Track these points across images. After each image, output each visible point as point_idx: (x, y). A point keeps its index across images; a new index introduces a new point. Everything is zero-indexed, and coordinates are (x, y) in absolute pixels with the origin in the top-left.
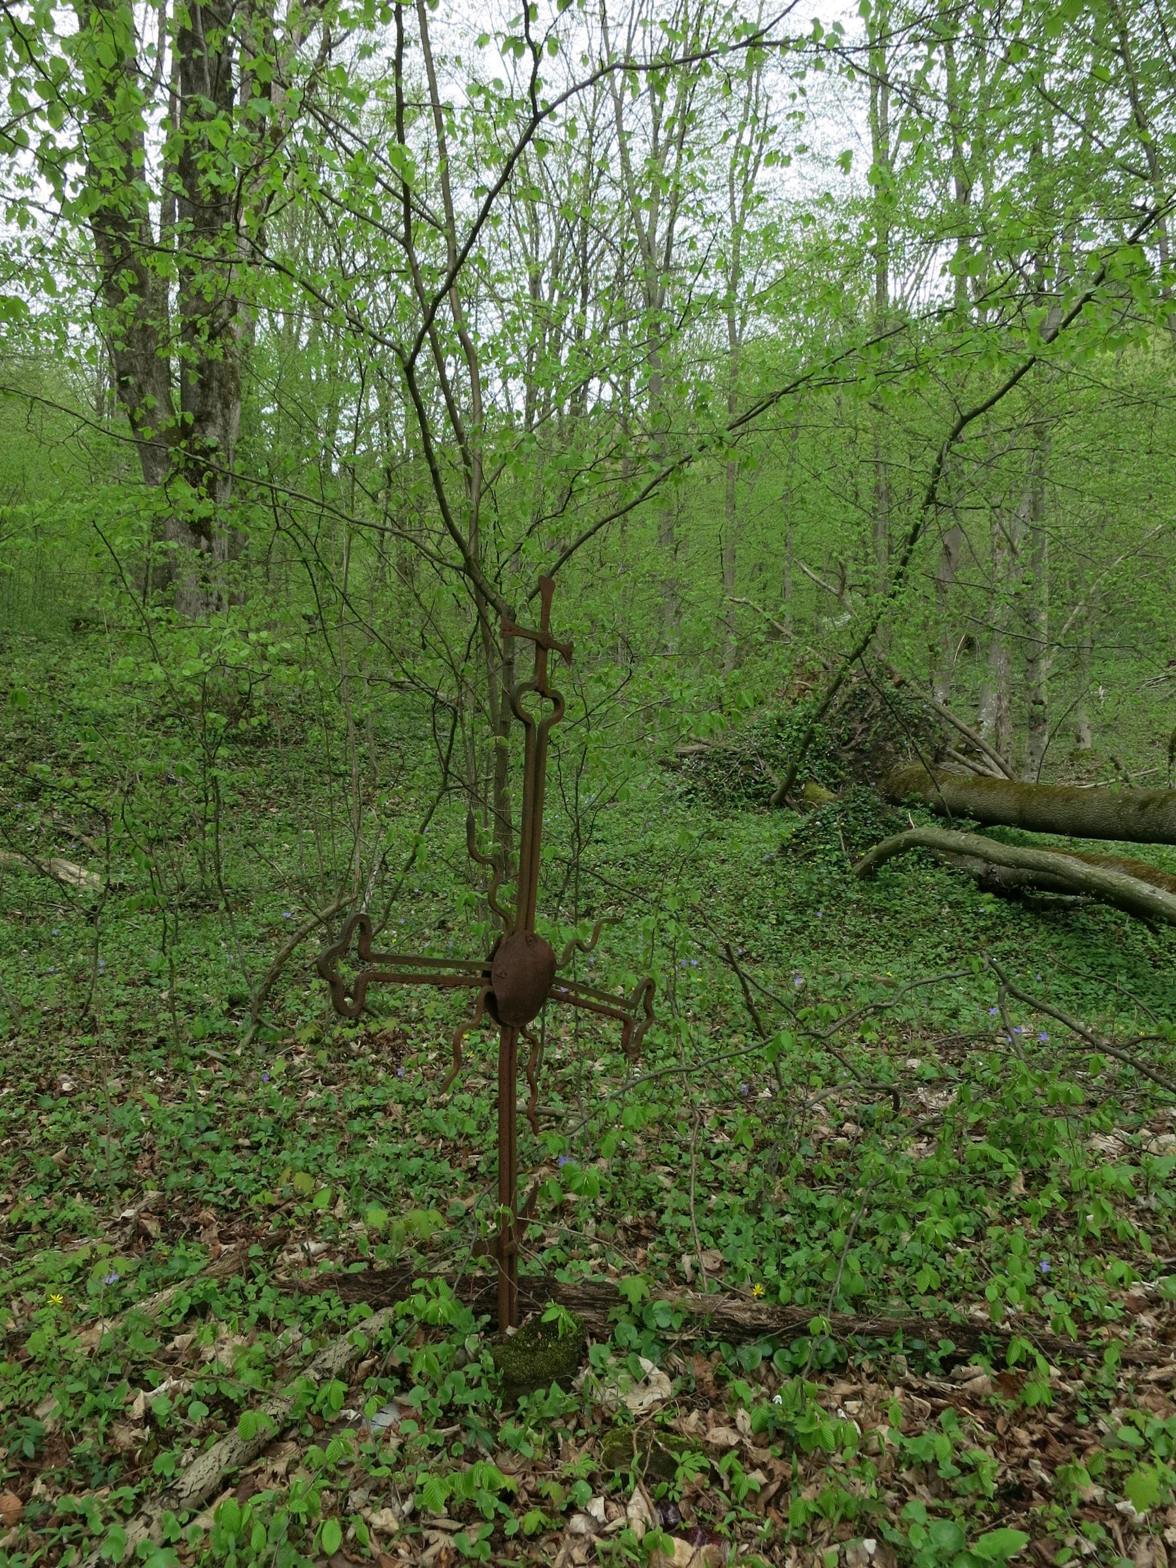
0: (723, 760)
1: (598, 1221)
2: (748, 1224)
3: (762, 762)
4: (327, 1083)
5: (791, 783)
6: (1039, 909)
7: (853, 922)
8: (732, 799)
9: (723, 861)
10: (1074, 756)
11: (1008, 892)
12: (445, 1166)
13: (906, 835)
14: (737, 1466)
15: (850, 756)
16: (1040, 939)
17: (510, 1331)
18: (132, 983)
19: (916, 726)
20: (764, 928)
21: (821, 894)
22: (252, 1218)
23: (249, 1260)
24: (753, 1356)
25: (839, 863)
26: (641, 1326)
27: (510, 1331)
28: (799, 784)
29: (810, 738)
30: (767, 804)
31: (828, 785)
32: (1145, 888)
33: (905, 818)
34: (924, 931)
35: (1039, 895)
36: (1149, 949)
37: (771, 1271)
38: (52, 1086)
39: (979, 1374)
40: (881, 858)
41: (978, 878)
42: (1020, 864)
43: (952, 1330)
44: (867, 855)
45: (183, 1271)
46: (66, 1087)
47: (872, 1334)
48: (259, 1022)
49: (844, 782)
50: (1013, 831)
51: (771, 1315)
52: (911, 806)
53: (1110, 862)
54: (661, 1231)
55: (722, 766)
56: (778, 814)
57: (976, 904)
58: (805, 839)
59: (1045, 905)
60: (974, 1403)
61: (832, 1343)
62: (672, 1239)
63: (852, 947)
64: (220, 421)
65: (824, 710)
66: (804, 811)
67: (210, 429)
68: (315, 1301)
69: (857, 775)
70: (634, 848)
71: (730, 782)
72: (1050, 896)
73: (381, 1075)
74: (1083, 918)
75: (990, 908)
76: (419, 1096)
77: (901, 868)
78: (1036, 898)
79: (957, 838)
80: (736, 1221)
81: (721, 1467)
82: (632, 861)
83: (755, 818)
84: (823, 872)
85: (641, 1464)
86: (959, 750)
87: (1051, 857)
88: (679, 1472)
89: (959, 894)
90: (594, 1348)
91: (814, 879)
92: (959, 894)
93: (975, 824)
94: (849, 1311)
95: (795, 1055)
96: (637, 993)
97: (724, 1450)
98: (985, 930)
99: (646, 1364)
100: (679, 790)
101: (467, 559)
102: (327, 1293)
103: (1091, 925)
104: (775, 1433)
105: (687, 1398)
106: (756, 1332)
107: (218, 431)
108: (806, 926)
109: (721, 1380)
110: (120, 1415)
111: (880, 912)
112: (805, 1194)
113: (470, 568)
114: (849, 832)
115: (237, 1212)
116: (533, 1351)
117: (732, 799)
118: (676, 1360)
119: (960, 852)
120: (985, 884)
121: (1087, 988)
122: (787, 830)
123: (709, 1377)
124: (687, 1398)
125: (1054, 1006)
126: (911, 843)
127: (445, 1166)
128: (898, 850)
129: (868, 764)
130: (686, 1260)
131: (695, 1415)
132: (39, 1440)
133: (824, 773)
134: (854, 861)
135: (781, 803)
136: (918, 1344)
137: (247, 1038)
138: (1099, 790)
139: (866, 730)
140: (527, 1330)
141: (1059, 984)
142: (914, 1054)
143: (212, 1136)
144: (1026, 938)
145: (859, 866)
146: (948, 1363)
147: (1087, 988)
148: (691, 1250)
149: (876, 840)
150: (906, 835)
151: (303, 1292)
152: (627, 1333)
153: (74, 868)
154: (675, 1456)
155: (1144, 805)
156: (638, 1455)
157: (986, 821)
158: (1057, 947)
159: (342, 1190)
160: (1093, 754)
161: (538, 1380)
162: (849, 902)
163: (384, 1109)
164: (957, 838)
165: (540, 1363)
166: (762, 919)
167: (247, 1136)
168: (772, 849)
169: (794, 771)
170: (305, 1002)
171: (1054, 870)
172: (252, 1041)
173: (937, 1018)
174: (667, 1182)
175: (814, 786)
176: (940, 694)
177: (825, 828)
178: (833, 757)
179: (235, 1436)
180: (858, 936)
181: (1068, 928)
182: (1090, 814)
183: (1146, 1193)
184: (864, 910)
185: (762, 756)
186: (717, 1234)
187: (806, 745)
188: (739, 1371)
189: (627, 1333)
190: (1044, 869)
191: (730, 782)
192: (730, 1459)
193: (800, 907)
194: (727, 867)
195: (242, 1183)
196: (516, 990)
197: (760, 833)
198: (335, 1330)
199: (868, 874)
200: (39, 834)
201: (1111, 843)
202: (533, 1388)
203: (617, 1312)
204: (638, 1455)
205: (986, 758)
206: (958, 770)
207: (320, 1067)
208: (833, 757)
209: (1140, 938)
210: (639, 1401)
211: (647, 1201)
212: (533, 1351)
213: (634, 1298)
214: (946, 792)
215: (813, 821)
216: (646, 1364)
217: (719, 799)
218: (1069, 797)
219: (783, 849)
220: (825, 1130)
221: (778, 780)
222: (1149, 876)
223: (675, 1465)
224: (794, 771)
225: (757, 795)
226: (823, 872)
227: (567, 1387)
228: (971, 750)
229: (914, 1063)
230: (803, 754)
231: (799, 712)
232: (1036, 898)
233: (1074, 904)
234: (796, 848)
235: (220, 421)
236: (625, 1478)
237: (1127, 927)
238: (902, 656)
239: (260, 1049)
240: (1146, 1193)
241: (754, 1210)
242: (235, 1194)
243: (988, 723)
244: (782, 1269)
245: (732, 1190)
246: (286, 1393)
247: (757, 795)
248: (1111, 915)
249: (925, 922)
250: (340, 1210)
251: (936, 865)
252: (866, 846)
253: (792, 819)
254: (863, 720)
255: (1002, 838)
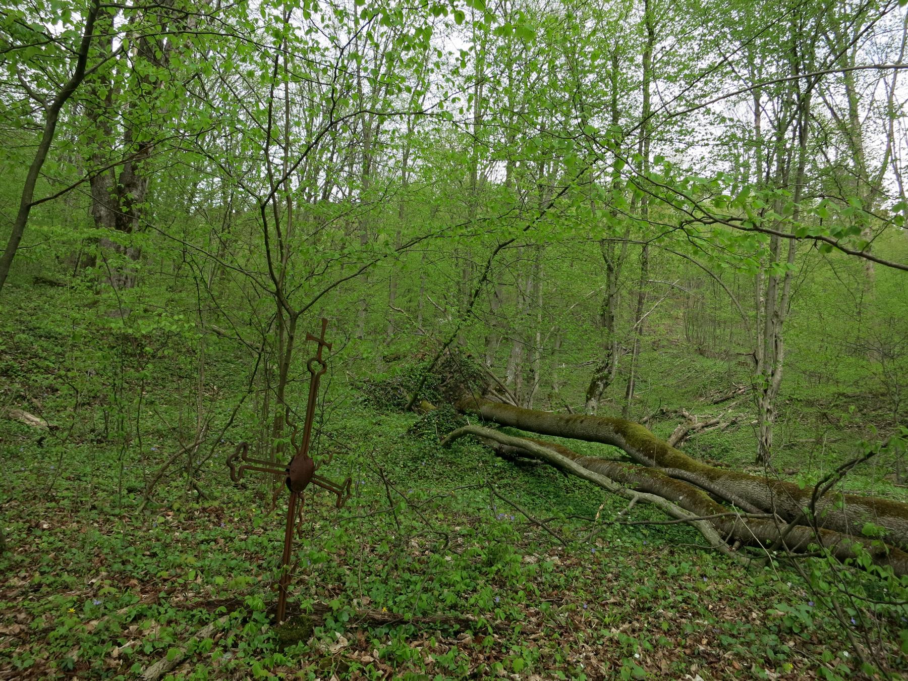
0: (384, 386)
1: (317, 587)
2: (382, 588)
3: (402, 389)
4: (185, 529)
5: (415, 399)
6: (521, 465)
7: (438, 468)
8: (386, 406)
9: (380, 436)
10: (550, 396)
11: (507, 457)
12: (247, 564)
13: (464, 428)
14: (373, 668)
15: (444, 389)
16: (520, 479)
17: (281, 623)
18: (69, 479)
19: (475, 376)
20: (397, 469)
21: (425, 454)
22: (155, 584)
23: (159, 599)
24: (381, 633)
25: (434, 440)
26: (336, 621)
27: (281, 623)
28: (419, 400)
29: (425, 380)
30: (403, 409)
31: (432, 402)
32: (560, 457)
33: (465, 420)
34: (470, 473)
35: (522, 459)
36: (565, 485)
37: (390, 603)
38: (38, 525)
39: (468, 637)
40: (453, 439)
41: (496, 450)
42: (511, 444)
43: (457, 620)
44: (447, 437)
45: (129, 602)
46: (45, 526)
47: (428, 623)
48: (148, 499)
49: (440, 402)
50: (514, 429)
51: (389, 616)
52: (470, 415)
53: (549, 445)
54: (345, 591)
55: (382, 389)
56: (408, 415)
57: (494, 462)
58: (420, 427)
59: (524, 464)
60: (465, 647)
61: (413, 627)
62: (349, 593)
63: (437, 479)
64: (140, 188)
65: (433, 366)
66: (420, 414)
67: (134, 191)
68: (195, 612)
69: (446, 398)
70: (337, 427)
71: (385, 398)
72: (527, 460)
73: (211, 526)
74: (540, 470)
75: (500, 464)
76: (232, 535)
77: (463, 444)
78: (519, 460)
79: (486, 431)
80: (377, 585)
81: (366, 669)
82: (335, 433)
83: (397, 416)
84: (427, 444)
85: (335, 667)
86: (496, 390)
87: (524, 441)
88: (350, 669)
89: (487, 457)
90: (316, 630)
91: (422, 446)
92: (487, 457)
93: (497, 425)
94: (420, 615)
95: (405, 524)
96: (345, 483)
97: (367, 664)
98: (497, 474)
99: (338, 634)
100: (360, 399)
101: (278, 290)
102: (199, 609)
103: (542, 474)
104: (388, 657)
105: (354, 647)
106: (382, 623)
107: (138, 193)
108: (417, 468)
109: (367, 641)
110: (108, 655)
111: (451, 464)
112: (407, 576)
113: (278, 293)
114: (439, 425)
115: (148, 582)
116: (291, 629)
117: (386, 406)
118: (350, 635)
119: (487, 437)
120: (499, 453)
121: (537, 501)
122: (412, 422)
123: (363, 639)
124: (354, 647)
125: (521, 508)
126: (466, 433)
127: (247, 564)
128: (461, 435)
129: (452, 394)
130: (355, 601)
131: (357, 652)
132: (74, 663)
133: (431, 396)
134: (441, 439)
135: (410, 409)
136: (446, 626)
137: (142, 507)
138: (551, 412)
139: (452, 377)
140: (290, 623)
141: (526, 499)
142: (458, 525)
143: (132, 549)
144: (514, 478)
145: (443, 442)
146: (456, 633)
147: (537, 501)
148: (357, 597)
149: (452, 429)
150: (464, 428)
151: (188, 609)
152: (331, 623)
153: (29, 416)
154: (349, 664)
155: (568, 421)
156: (334, 664)
157: (503, 424)
158: (527, 482)
159: (199, 573)
160: (558, 396)
161: (294, 641)
162: (438, 458)
163: (215, 541)
164: (486, 431)
165: (294, 634)
166: (396, 464)
167: (148, 550)
168: (403, 431)
169: (416, 395)
170: (168, 492)
171: (524, 447)
172: (144, 509)
173: (470, 510)
174: (348, 572)
175: (425, 402)
176: (489, 363)
177: (429, 423)
178: (436, 389)
179: (165, 659)
180: (440, 474)
181: (533, 475)
182: (546, 424)
183: (541, 576)
184: (445, 462)
185: (402, 386)
186: (369, 590)
187: (422, 383)
188: (375, 637)
189: (331, 623)
190: (516, 445)
191: (385, 398)
192: (369, 666)
193: (415, 460)
194: (382, 439)
195: (152, 569)
196: (299, 479)
197: (398, 423)
198: (203, 623)
199: (447, 445)
200: (6, 395)
201: (557, 438)
202: (290, 645)
203: (328, 615)
204: (334, 664)
205: (507, 394)
206: (493, 398)
207: (180, 522)
208: (436, 389)
209: (562, 481)
210: (335, 649)
211: (339, 579)
212: (291, 629)
213: (335, 608)
214: (485, 409)
215: (423, 419)
216: (338, 634)
217: (380, 405)
218: (538, 415)
219: (409, 431)
220: (417, 553)
221: (409, 398)
222: (564, 452)
223: (348, 667)
224: (416, 395)
225: (399, 404)
226: (427, 444)
227: (305, 643)
228: (501, 390)
229: (458, 528)
230: (421, 388)
231: (421, 365)
232: (519, 460)
233: (536, 464)
234: (415, 432)
235: (140, 188)
236: (329, 673)
237: (557, 475)
238: (470, 347)
239: (147, 513)
240: (541, 576)
241: (385, 582)
242: (146, 574)
243: (510, 378)
244: (395, 603)
245: (376, 575)
246: (186, 645)
247: (399, 404)
248: (551, 470)
249: (471, 469)
250: (199, 580)
251: (478, 443)
252: (447, 433)
253: (414, 417)
254: (450, 372)
255: (508, 433)
